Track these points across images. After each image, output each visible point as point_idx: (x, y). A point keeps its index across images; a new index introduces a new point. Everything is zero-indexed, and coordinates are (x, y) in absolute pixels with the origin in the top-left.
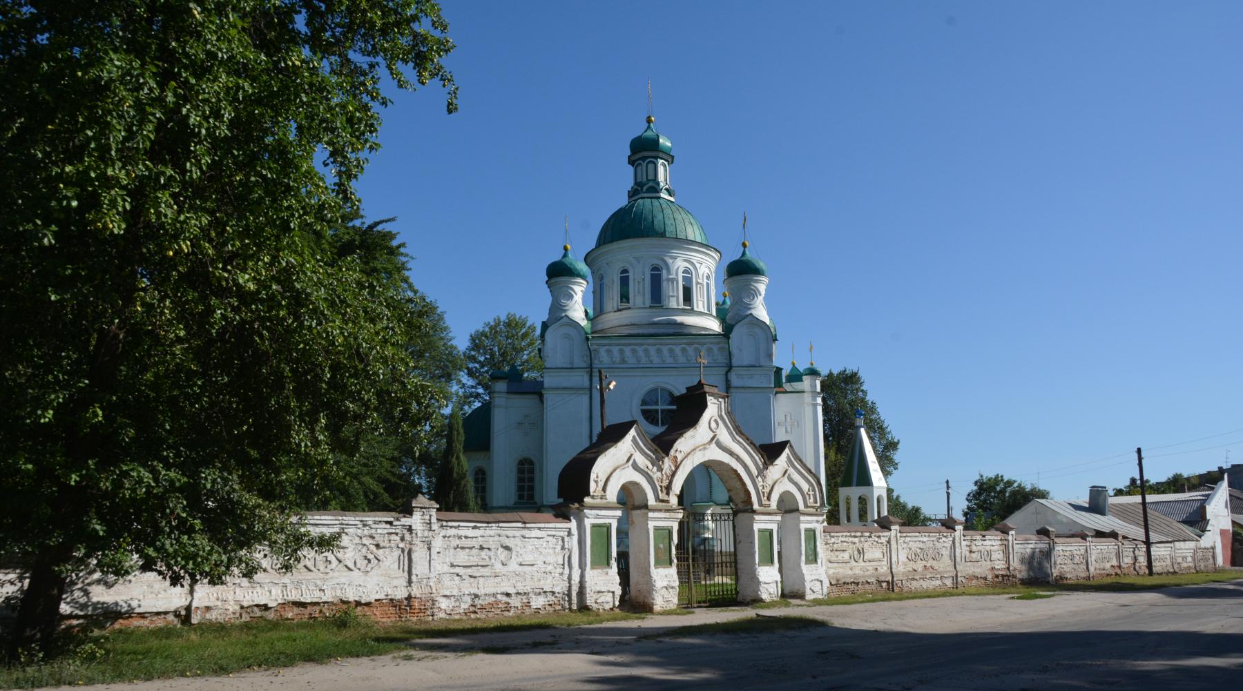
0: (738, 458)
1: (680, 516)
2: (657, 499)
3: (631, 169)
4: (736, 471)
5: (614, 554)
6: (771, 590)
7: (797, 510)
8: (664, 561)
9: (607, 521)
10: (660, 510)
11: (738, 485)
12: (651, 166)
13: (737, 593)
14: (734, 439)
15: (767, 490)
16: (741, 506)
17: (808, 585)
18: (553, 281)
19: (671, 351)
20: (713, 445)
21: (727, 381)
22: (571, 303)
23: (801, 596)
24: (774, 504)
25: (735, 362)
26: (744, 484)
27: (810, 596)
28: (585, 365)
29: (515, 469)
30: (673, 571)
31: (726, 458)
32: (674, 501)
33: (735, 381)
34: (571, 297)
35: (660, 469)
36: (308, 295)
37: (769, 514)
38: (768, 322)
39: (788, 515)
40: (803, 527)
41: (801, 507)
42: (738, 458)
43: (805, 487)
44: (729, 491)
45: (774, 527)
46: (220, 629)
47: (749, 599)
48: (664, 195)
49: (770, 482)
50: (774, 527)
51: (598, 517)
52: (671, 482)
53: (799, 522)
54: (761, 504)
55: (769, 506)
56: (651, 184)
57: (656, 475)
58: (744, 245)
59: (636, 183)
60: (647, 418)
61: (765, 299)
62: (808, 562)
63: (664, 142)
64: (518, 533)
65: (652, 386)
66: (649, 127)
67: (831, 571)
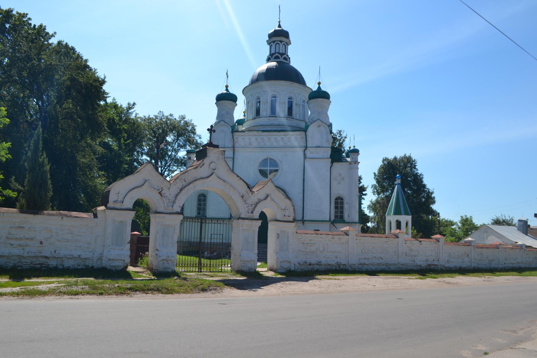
3: (268, 47)
5: (58, 212)
19: (276, 139)
21: (305, 155)
25: (309, 145)
28: (231, 146)
29: (196, 200)
33: (308, 154)
36: (51, 64)
46: (34, 277)
56: (277, 54)
64: (506, 265)
65: (265, 157)
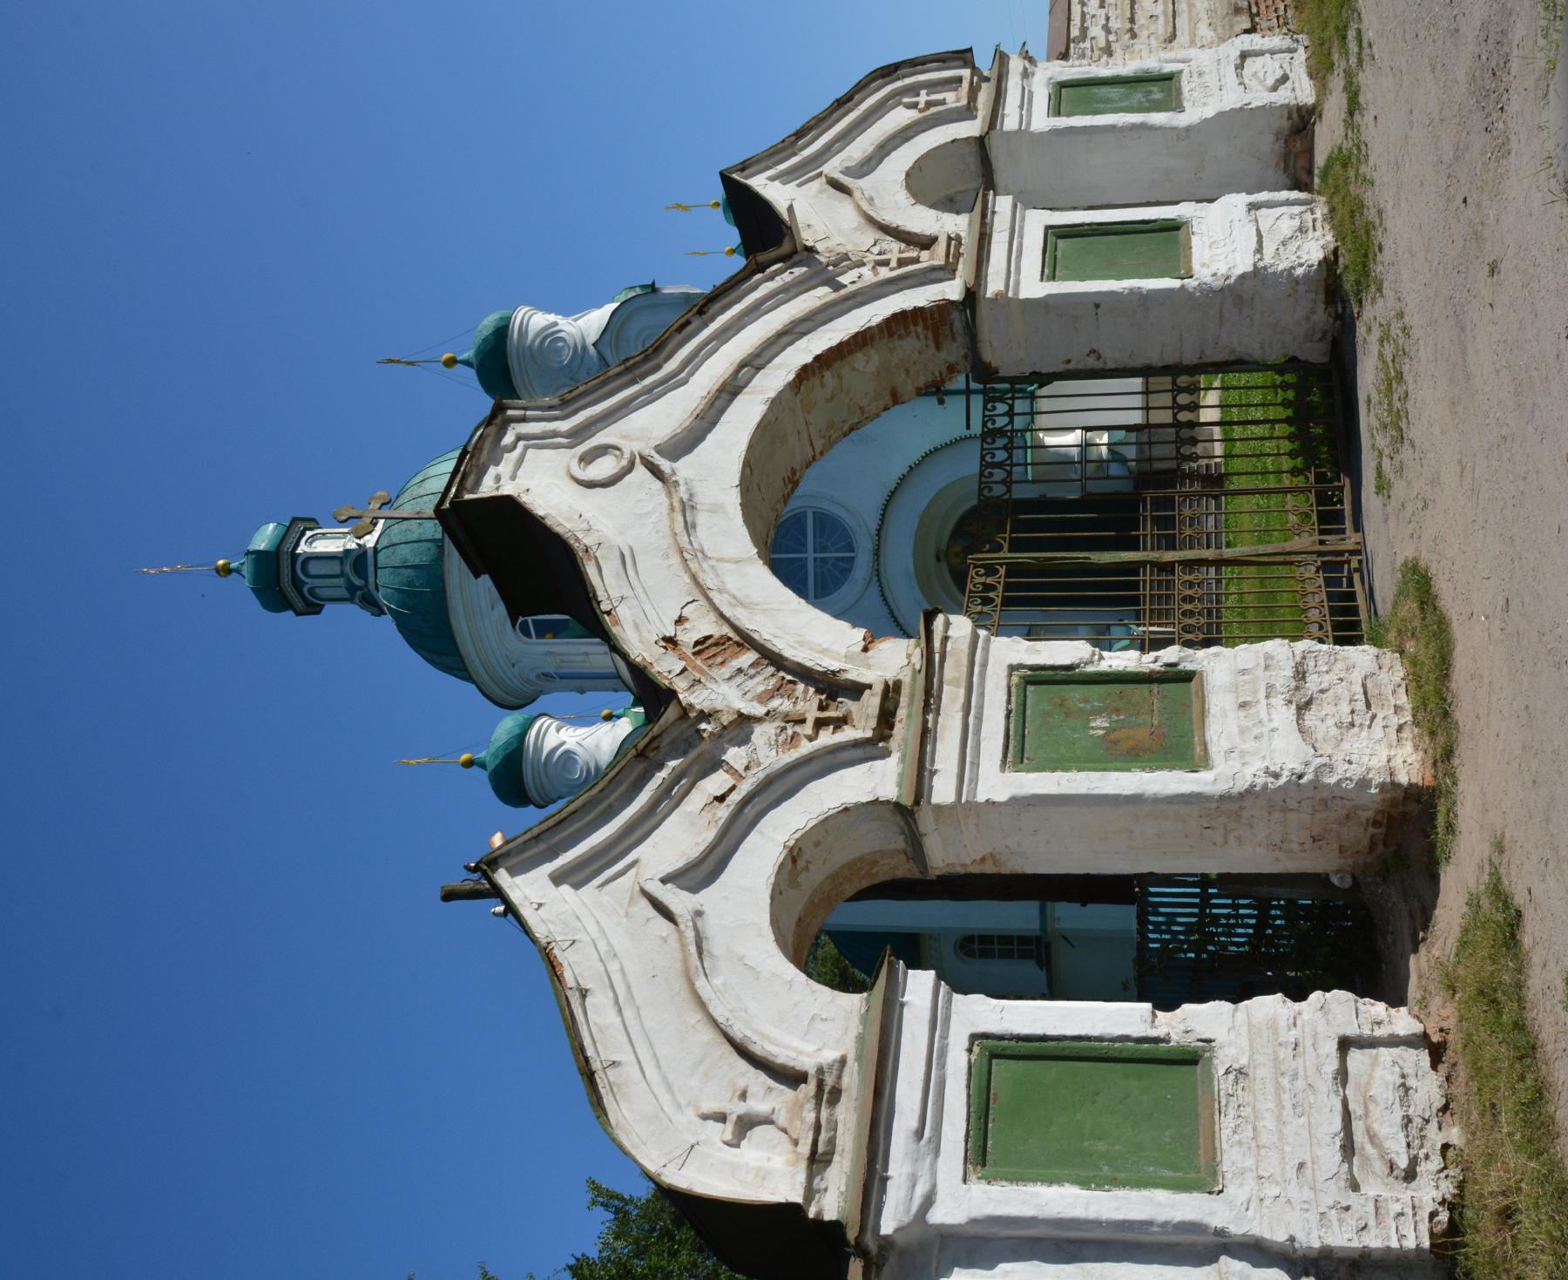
0: (755, 362)
1: (961, 626)
2: (872, 748)
3: (329, 608)
4: (804, 373)
5: (1125, 1018)
6: (1287, 226)
7: (981, 142)
8: (1166, 720)
9: (958, 1061)
10: (926, 736)
11: (866, 363)
12: (314, 568)
13: (1293, 363)
14: (675, 381)
15: (894, 249)
16: (954, 351)
17: (1260, 97)
18: (533, 794)
20: (684, 469)
22: (582, 757)
23: (1302, 122)
24: (958, 224)
26: (862, 340)
27: (1303, 91)
30: (1220, 667)
31: (746, 414)
32: (894, 659)
34: (569, 756)
35: (742, 726)
37: (984, 239)
38: (613, 306)
39: (1000, 177)
40: (1041, 121)
41: (970, 129)
42: (755, 362)
43: (900, 117)
44: (896, 399)
45: (1036, 222)
47: (1321, 316)
48: (370, 541)
49: (862, 241)
50: (1036, 222)
51: (927, 1134)
52: (804, 674)
53: (1023, 133)
54: (946, 271)
55: (954, 240)
56: (348, 569)
57: (764, 752)
58: (451, 362)
59: (351, 600)
60: (838, 584)
61: (567, 312)
62: (1173, 102)
63: (264, 537)
66: (238, 571)
67: (1205, 32)
